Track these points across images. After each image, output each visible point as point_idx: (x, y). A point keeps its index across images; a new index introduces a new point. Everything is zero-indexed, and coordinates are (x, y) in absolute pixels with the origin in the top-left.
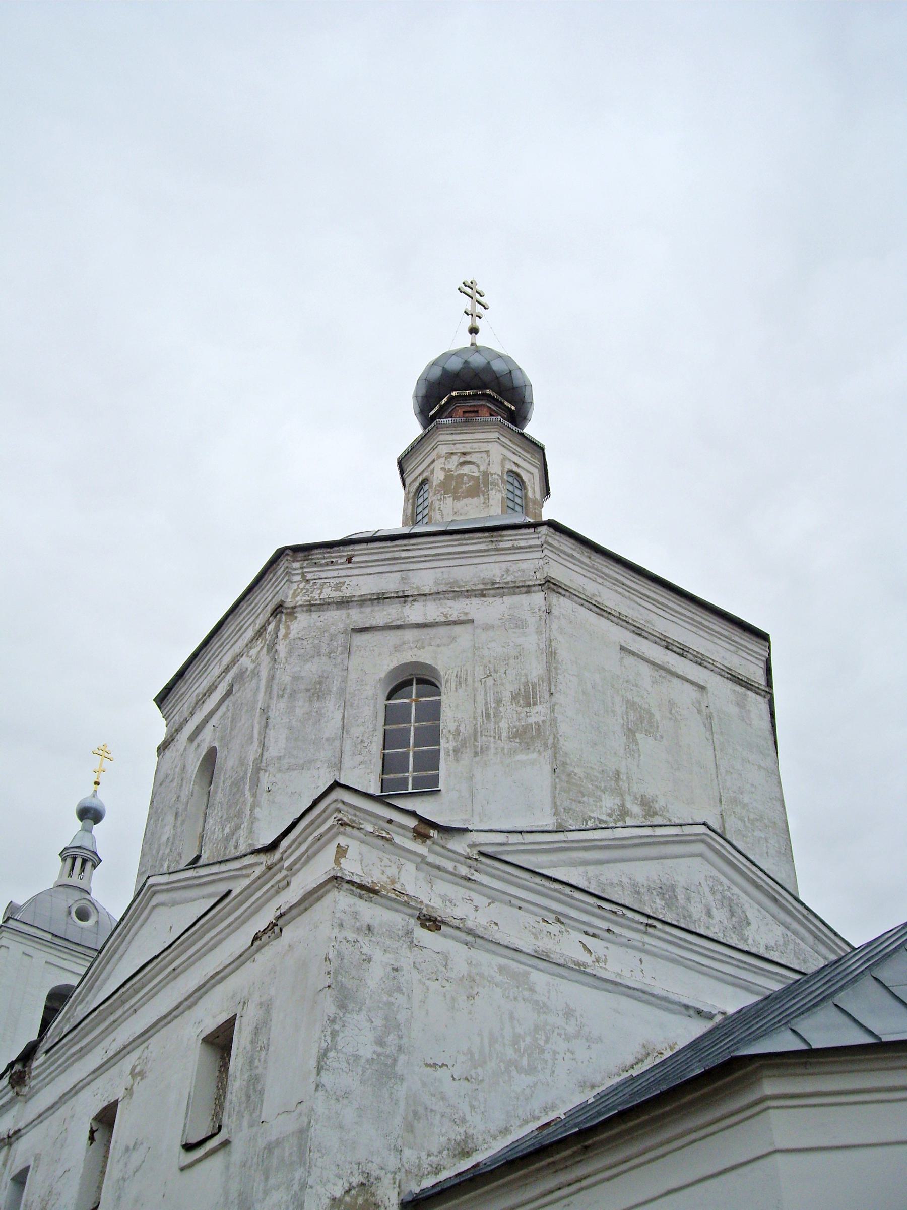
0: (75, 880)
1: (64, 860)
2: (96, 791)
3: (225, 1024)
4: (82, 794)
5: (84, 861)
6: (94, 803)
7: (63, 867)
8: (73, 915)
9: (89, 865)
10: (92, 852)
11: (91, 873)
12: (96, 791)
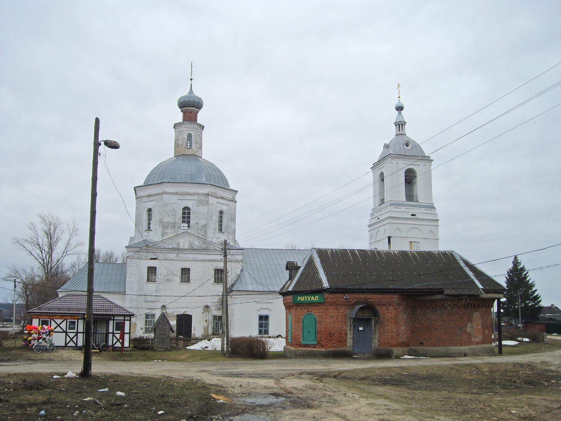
0: (401, 132)
1: (396, 125)
2: (399, 100)
3: (136, 221)
4: (395, 103)
5: (402, 125)
6: (399, 105)
7: (396, 129)
8: (405, 145)
9: (403, 126)
10: (404, 122)
11: (405, 127)
12: (399, 100)
